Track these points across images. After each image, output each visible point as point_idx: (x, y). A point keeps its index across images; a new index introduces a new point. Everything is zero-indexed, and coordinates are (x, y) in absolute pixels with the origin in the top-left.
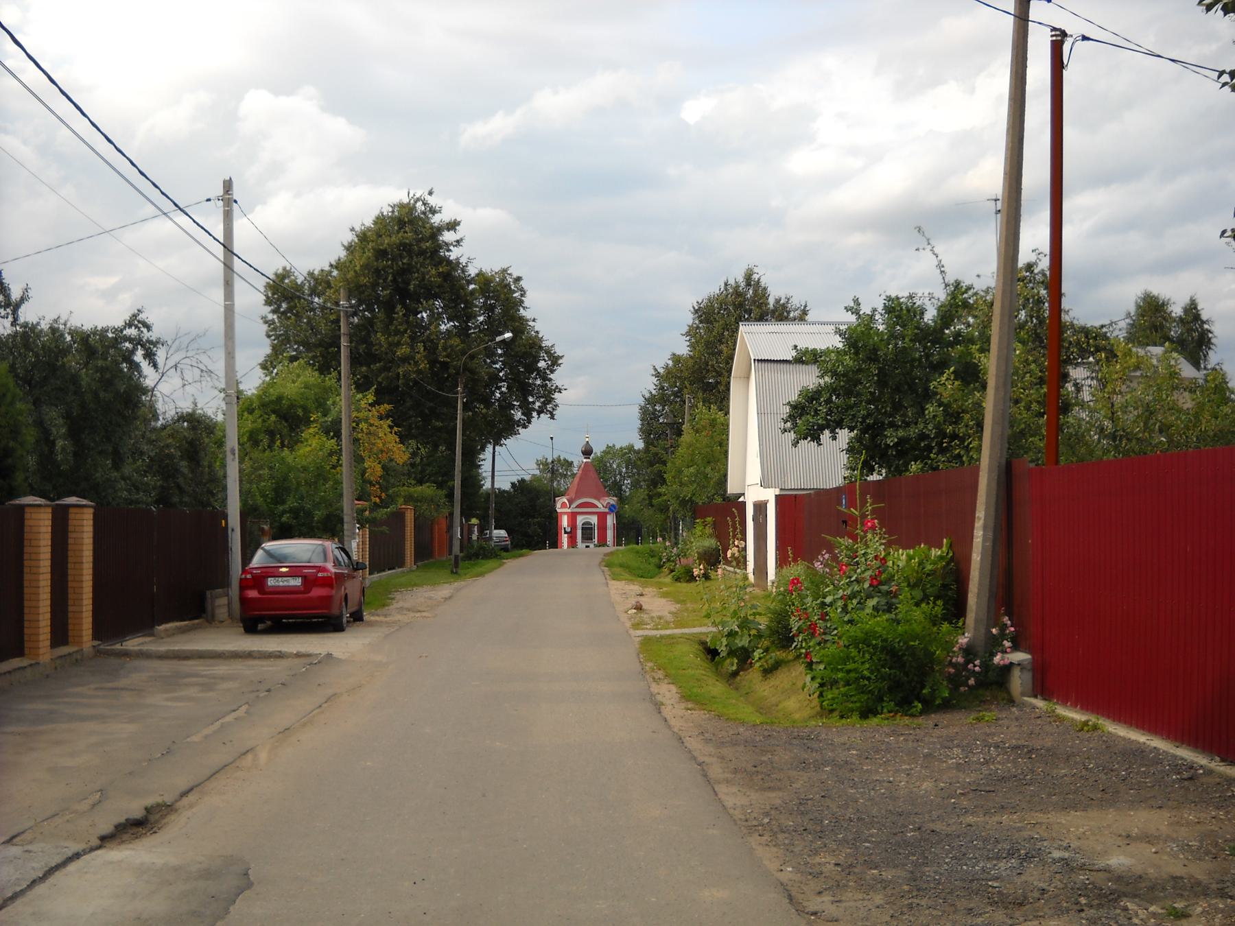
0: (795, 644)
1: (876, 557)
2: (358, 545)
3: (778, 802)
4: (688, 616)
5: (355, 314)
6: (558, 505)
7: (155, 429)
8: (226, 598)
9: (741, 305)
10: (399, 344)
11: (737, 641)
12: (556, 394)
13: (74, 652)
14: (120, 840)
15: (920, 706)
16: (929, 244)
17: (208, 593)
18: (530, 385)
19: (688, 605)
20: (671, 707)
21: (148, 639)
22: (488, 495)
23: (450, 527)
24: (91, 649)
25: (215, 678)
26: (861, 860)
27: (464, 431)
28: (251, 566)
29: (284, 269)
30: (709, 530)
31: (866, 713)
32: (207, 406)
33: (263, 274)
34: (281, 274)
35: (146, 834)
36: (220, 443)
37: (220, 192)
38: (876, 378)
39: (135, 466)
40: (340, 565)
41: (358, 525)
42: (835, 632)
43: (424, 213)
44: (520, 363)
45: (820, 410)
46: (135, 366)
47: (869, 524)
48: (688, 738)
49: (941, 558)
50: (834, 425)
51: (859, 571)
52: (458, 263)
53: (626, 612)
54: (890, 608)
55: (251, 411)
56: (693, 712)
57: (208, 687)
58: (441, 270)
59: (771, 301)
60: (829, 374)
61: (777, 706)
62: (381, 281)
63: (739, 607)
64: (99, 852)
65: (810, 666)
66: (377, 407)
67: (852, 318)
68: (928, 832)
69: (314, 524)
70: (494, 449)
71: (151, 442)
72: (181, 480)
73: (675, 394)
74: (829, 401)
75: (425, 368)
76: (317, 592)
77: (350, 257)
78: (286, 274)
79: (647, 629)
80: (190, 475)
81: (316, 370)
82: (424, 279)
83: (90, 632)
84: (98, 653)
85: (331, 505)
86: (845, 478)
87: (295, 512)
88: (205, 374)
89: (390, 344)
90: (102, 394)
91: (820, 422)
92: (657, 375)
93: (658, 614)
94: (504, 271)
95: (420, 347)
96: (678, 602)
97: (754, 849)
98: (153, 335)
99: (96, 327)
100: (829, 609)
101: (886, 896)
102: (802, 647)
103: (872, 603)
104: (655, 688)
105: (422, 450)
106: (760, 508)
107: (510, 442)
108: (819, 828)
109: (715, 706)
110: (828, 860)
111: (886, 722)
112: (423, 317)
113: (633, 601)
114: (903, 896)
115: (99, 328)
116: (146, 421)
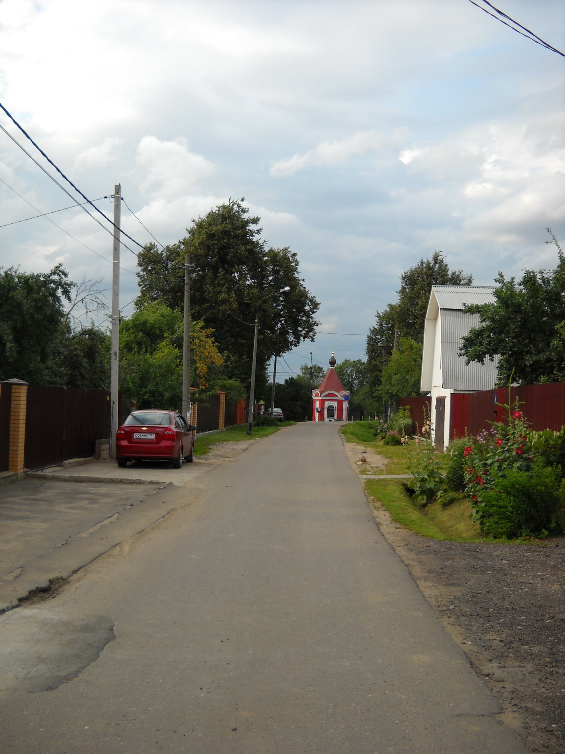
0: (467, 489)
1: (521, 435)
2: (191, 415)
3: (459, 594)
4: (395, 467)
5: (194, 271)
6: (314, 395)
7: (68, 339)
8: (108, 445)
9: (431, 275)
10: (220, 292)
11: (427, 485)
12: (315, 326)
13: (12, 475)
14: (31, 602)
15: (547, 533)
16: (554, 239)
17: (97, 441)
18: (299, 320)
19: (394, 460)
20: (386, 526)
21: (58, 469)
22: (270, 387)
23: (247, 406)
24: (23, 474)
25: (98, 495)
26: (517, 638)
27: (258, 349)
28: (124, 425)
29: (151, 244)
30: (407, 414)
31: (512, 535)
32: (100, 325)
33: (138, 244)
34: (148, 247)
35: (49, 597)
36: (108, 349)
37: (113, 193)
38: (519, 323)
39: (54, 361)
40: (179, 427)
41: (191, 403)
42: (493, 483)
43: (238, 212)
44: (294, 307)
45: (483, 343)
46: (58, 299)
47: (517, 414)
48: (398, 548)
49: (559, 437)
50: (492, 352)
51: (509, 444)
52: (258, 244)
53: (356, 463)
54: (528, 469)
55: (128, 330)
56: (400, 530)
57: (93, 501)
58: (248, 247)
59: (450, 273)
60: (490, 320)
61: (452, 527)
62: (211, 252)
63: (429, 463)
64: (17, 610)
65: (476, 503)
66: (206, 330)
67: (498, 285)
68: (559, 620)
69: (164, 401)
70: (276, 358)
71: (65, 346)
72: (83, 371)
73: (389, 329)
74: (489, 336)
75: (236, 307)
76: (164, 443)
77: (192, 238)
78: (152, 247)
79: (369, 474)
80: (89, 368)
81: (168, 306)
82: (237, 253)
83: (23, 463)
84: (27, 476)
85: (175, 389)
86: (495, 384)
87: (152, 393)
88: (100, 305)
89: (215, 292)
90: (36, 316)
91: (483, 350)
92: (379, 317)
93: (377, 465)
94: (286, 249)
95: (233, 294)
96: (388, 457)
97: (445, 627)
98: (68, 280)
99: (33, 274)
100: (489, 467)
101: (535, 664)
102: (471, 492)
103: (517, 465)
104: (375, 513)
105: (232, 357)
106: (441, 401)
107: (286, 355)
108: (487, 614)
109: (414, 526)
110: (495, 637)
111: (525, 542)
112: (235, 276)
113: (360, 456)
114: (546, 666)
115: (35, 274)
116: (63, 333)
